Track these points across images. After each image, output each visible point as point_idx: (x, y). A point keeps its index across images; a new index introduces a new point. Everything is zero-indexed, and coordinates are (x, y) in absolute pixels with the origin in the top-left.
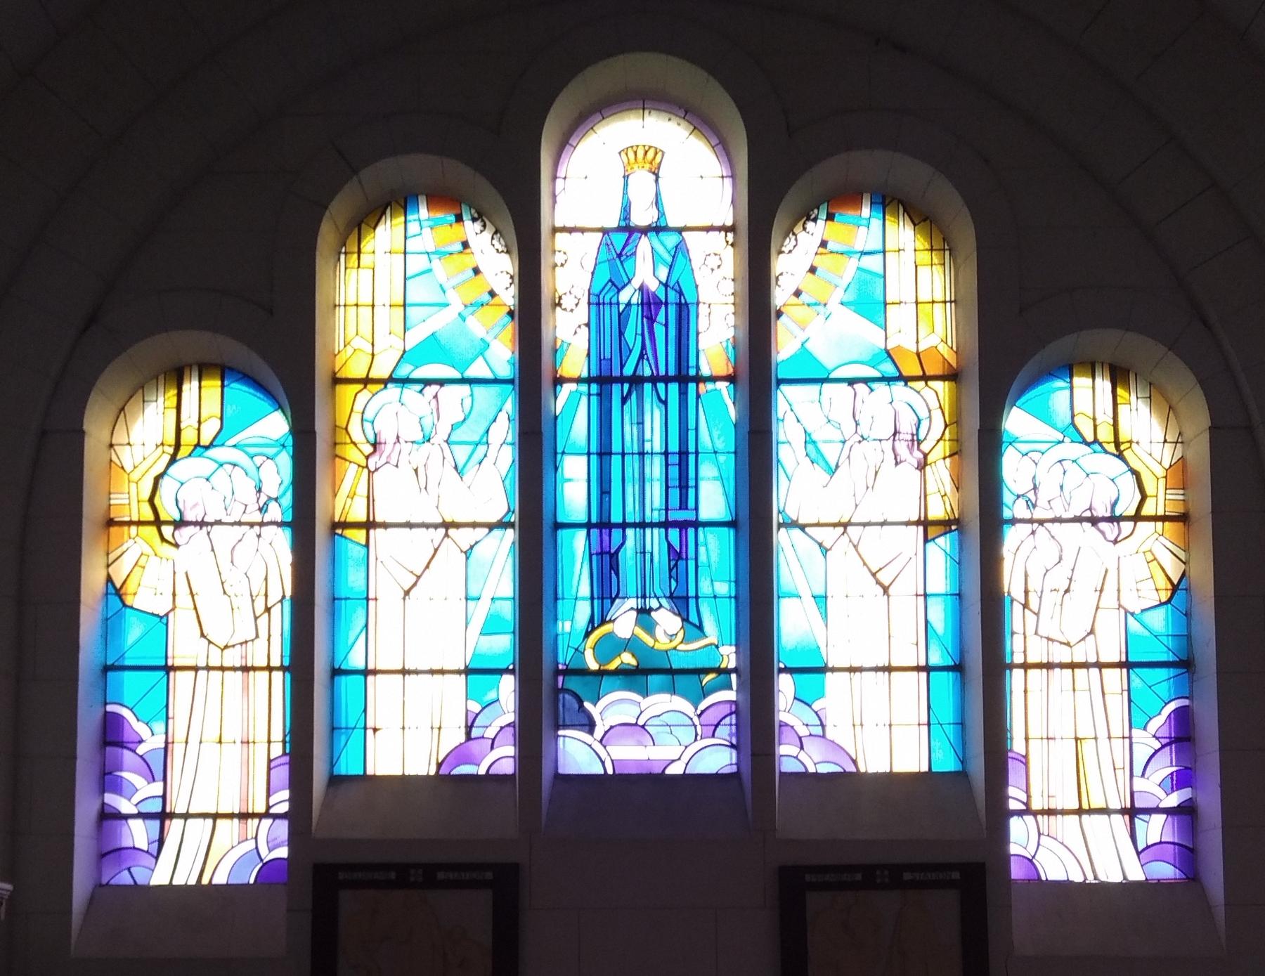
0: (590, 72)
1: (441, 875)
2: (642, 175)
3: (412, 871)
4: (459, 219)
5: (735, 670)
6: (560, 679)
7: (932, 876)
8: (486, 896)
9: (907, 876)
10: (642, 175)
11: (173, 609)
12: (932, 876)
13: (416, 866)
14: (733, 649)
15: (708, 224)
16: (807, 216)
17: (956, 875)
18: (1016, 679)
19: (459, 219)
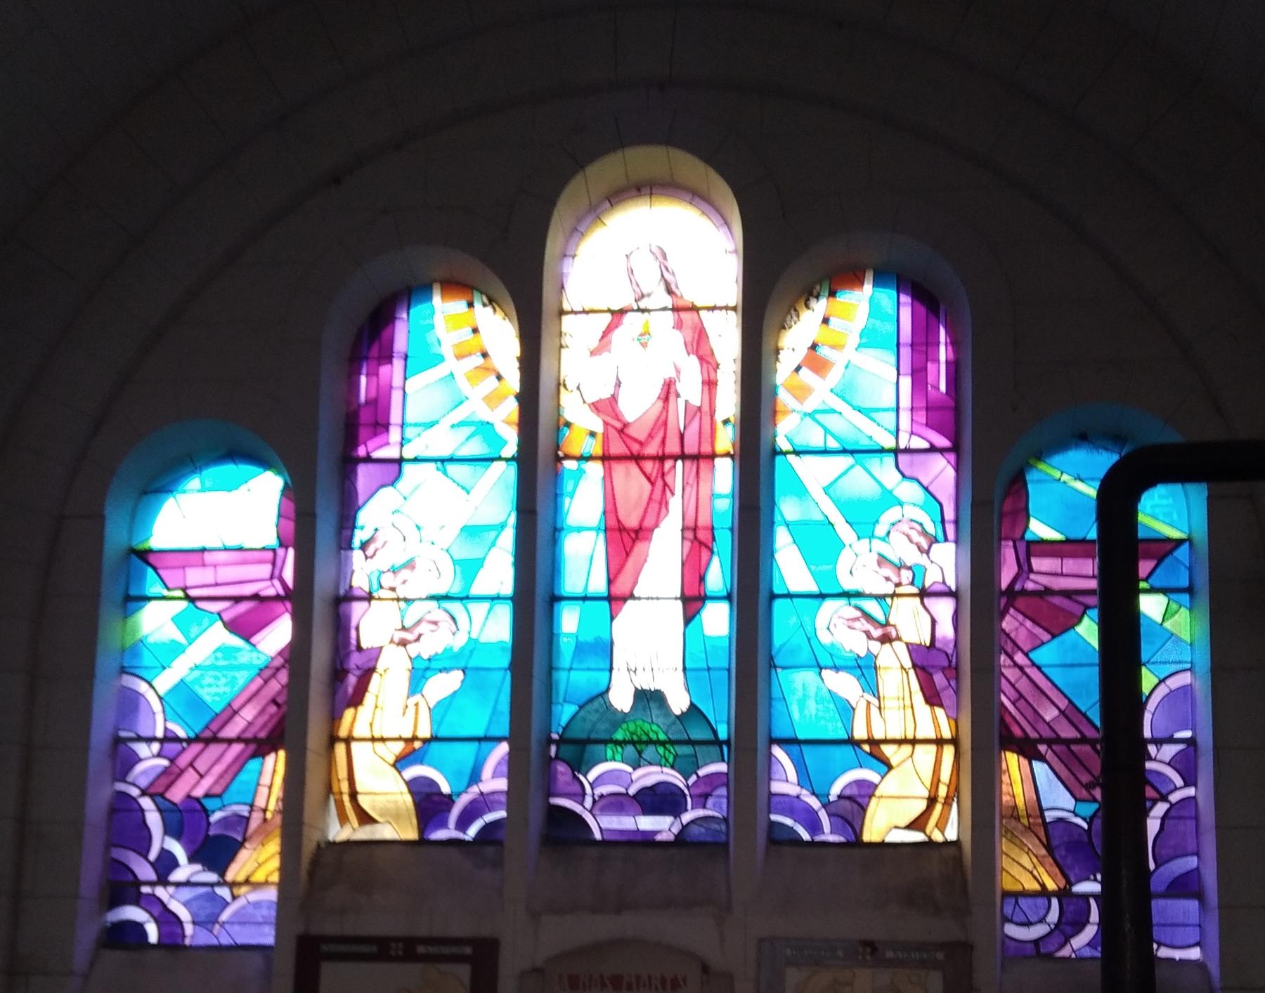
0: (593, 170)
1: (421, 949)
2: (651, 266)
3: (393, 945)
4: (471, 305)
5: (728, 742)
6: (553, 749)
7: (446, 950)
8: (464, 971)
9: (421, 949)
10: (651, 266)
11: (896, 827)
12: (446, 950)
13: (397, 939)
14: (561, 677)
15: (712, 304)
16: (809, 295)
17: (468, 950)
18: (508, 588)
19: (471, 305)
